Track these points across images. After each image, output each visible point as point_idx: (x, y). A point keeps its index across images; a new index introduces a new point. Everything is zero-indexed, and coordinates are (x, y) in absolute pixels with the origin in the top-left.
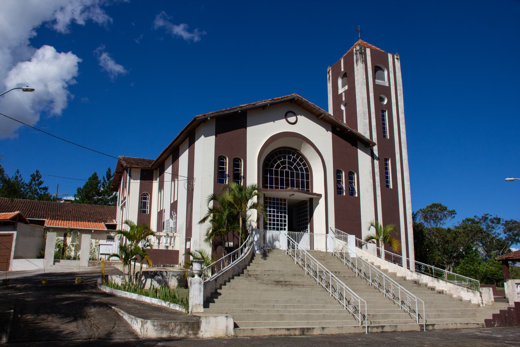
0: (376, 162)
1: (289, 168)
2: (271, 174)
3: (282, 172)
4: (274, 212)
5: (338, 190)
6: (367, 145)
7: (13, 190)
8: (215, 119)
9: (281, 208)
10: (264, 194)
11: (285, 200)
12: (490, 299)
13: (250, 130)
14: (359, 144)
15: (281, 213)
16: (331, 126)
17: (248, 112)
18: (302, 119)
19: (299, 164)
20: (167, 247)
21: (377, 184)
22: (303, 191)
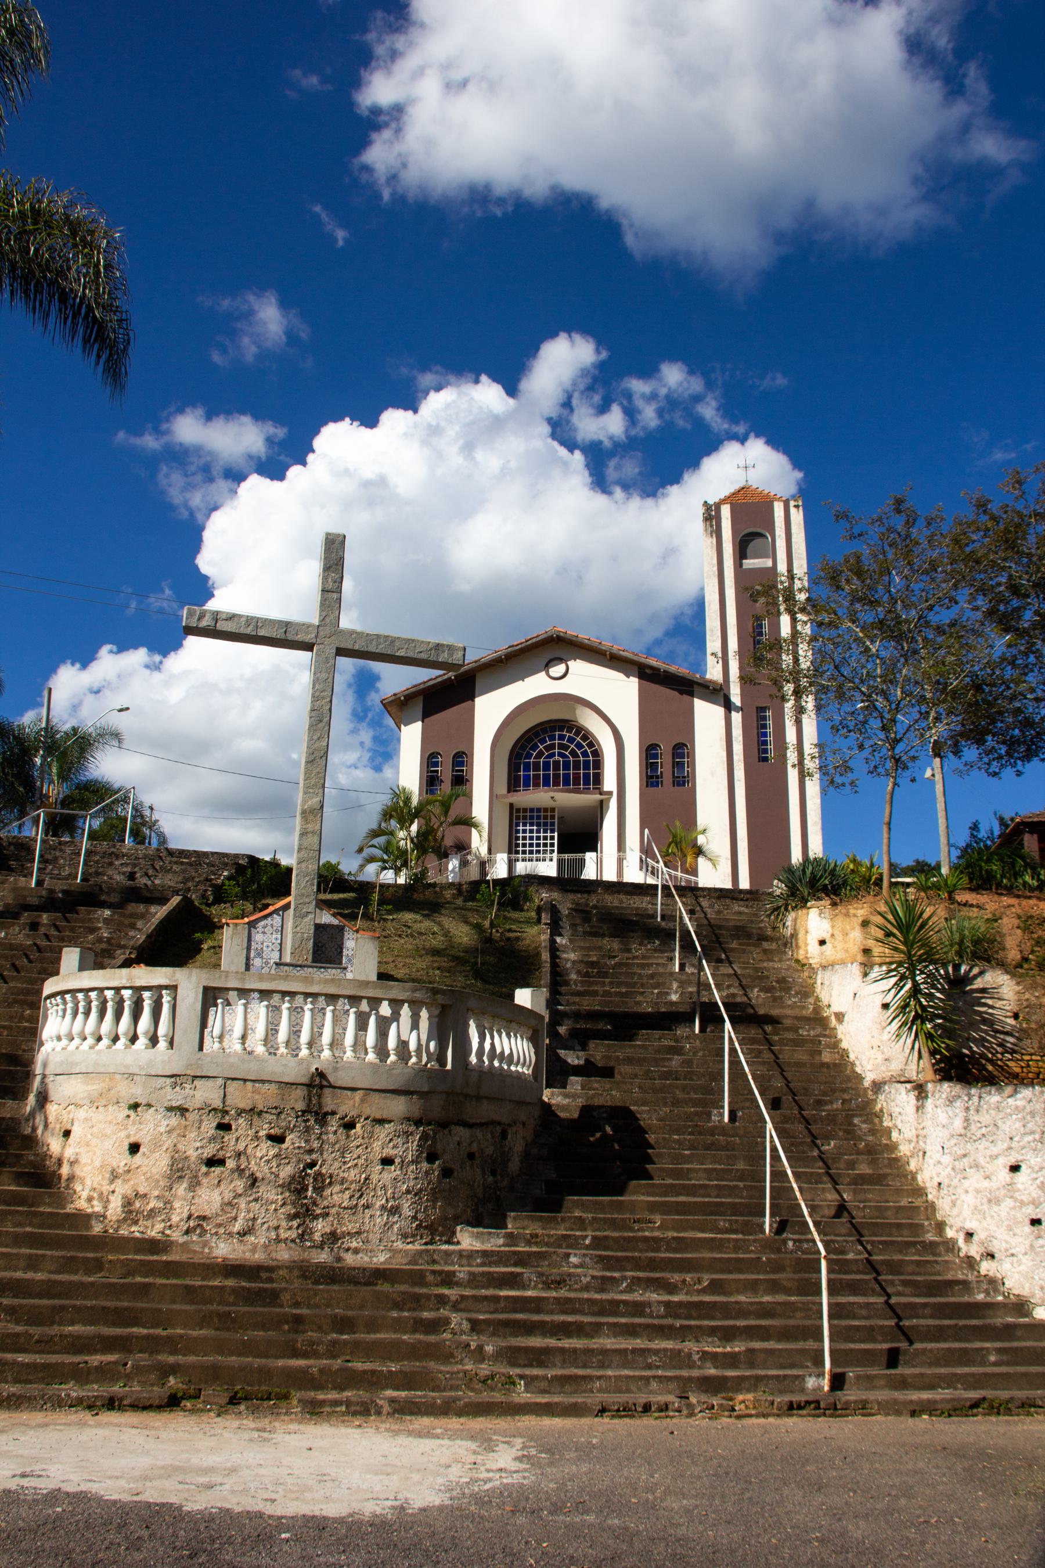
0: (737, 717)
1: (561, 755)
2: (527, 768)
4: (531, 831)
5: (650, 778)
6: (717, 693)
8: (421, 698)
9: (545, 824)
10: (511, 805)
11: (553, 810)
12: (795, 920)
13: (482, 703)
14: (696, 689)
15: (525, 825)
16: (636, 669)
17: (478, 675)
18: (579, 667)
19: (579, 746)
20: (132, 876)
21: (735, 758)
22: (586, 791)
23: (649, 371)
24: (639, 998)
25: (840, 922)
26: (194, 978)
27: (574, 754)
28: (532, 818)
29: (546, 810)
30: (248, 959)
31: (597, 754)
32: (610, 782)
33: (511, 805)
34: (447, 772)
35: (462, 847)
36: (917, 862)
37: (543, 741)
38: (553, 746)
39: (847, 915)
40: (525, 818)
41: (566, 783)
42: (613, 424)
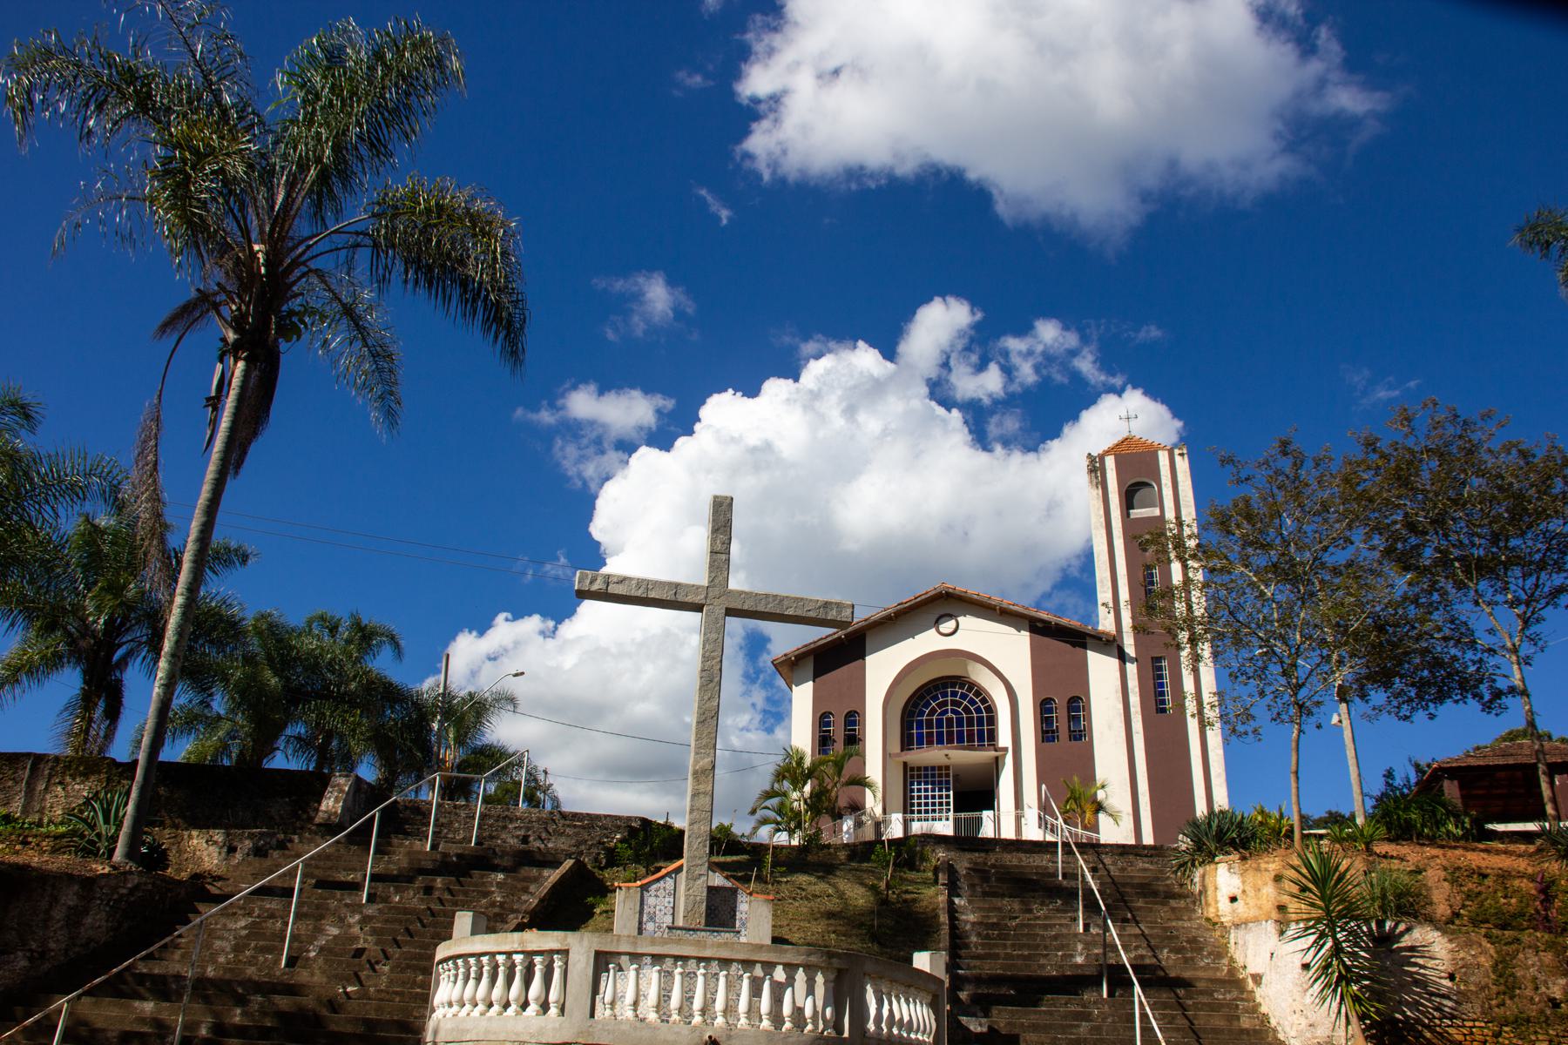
0: (1132, 668)
1: (953, 711)
2: (920, 726)
3: (940, 722)
4: (926, 790)
5: (1046, 733)
6: (1110, 645)
7: (14, 759)
8: (811, 659)
9: (940, 783)
10: (905, 764)
11: (947, 768)
12: (1203, 876)
14: (1089, 640)
18: (968, 622)
19: (972, 702)
22: (981, 747)
23: (1024, 329)
24: (1042, 961)
25: (1250, 876)
26: (586, 943)
27: (967, 710)
28: (926, 776)
29: (940, 768)
30: (640, 923)
31: (991, 710)
32: (1004, 738)
33: (905, 764)
34: (839, 731)
35: (856, 808)
36: (1330, 813)
37: (935, 698)
38: (945, 703)
39: (1258, 869)
40: (919, 776)
41: (960, 740)
42: (991, 382)
